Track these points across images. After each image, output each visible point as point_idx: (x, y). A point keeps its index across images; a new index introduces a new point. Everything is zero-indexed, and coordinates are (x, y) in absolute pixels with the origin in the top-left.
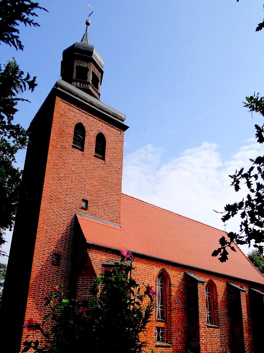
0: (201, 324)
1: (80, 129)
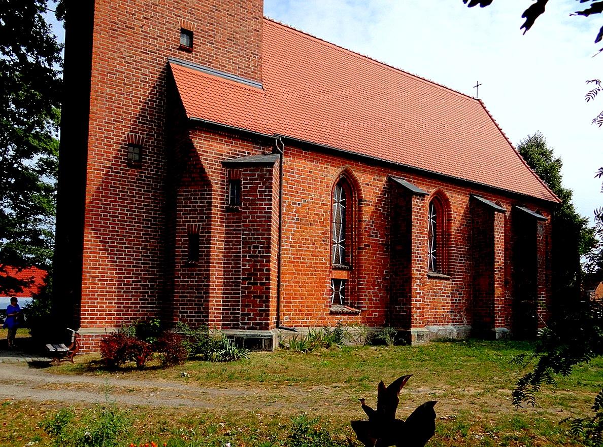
0: (415, 272)
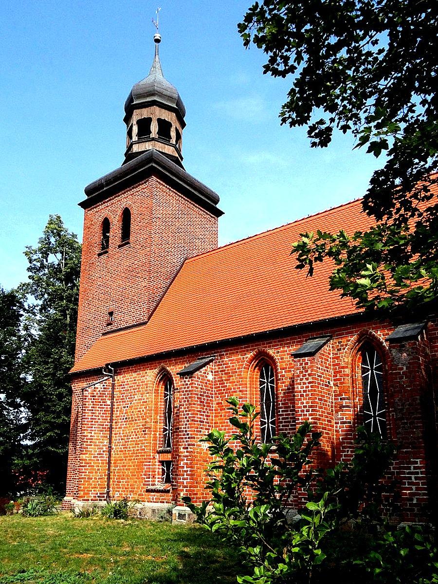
0: (182, 450)
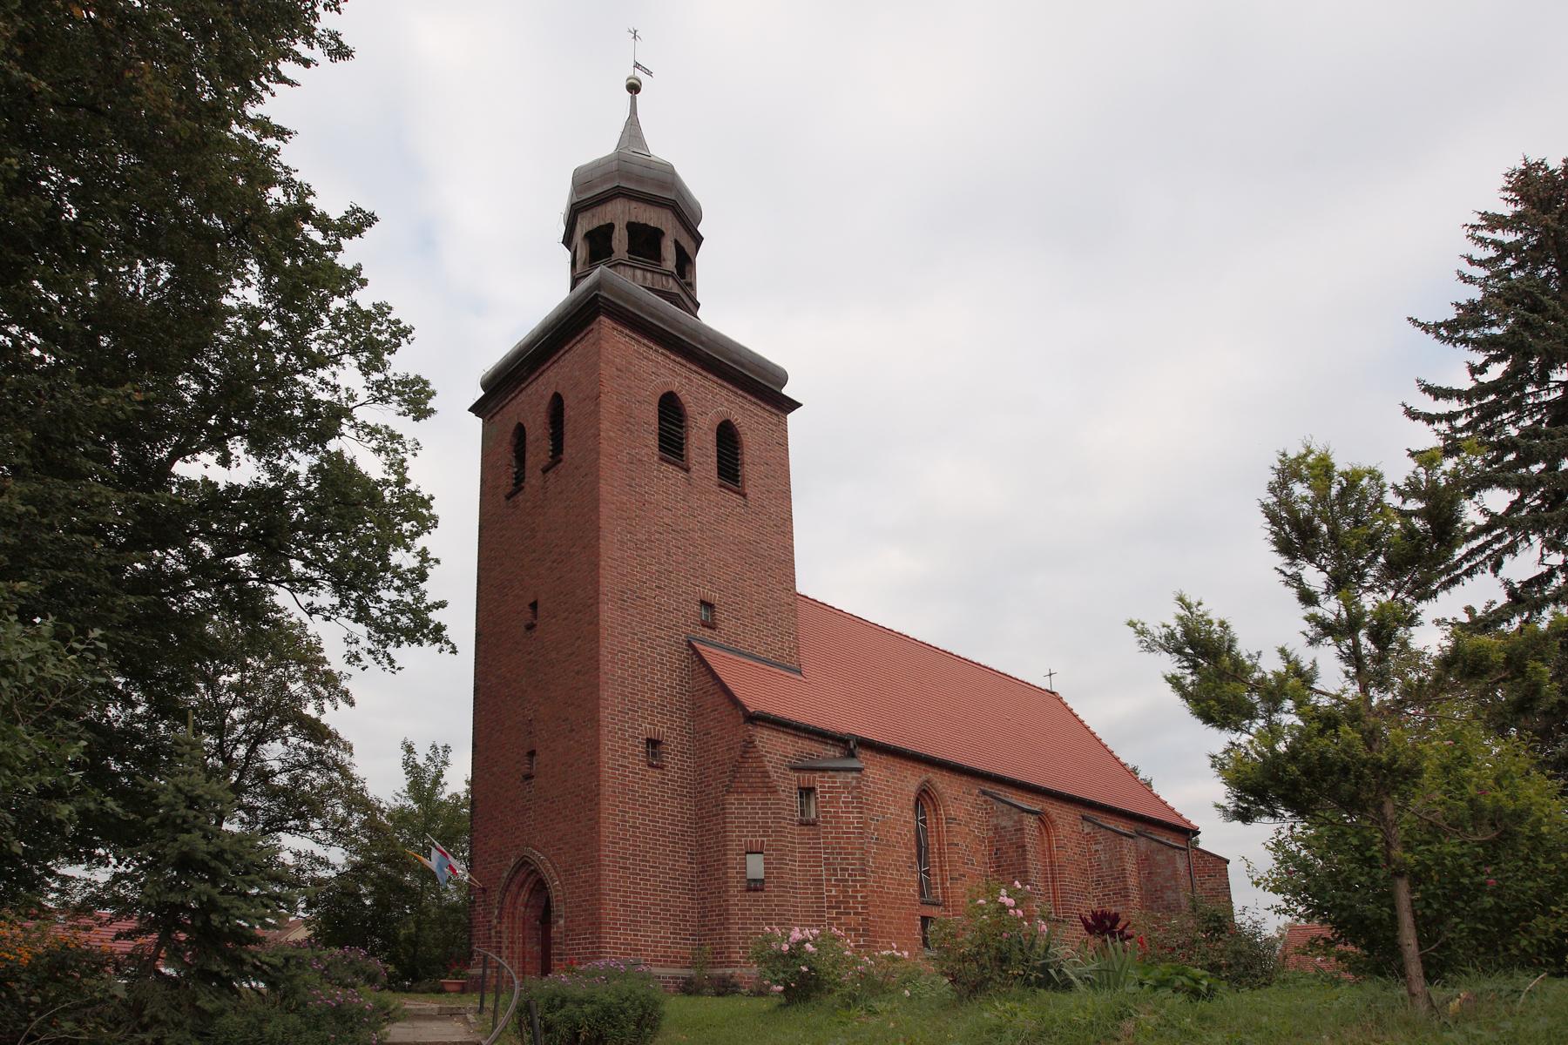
1: (670, 408)
